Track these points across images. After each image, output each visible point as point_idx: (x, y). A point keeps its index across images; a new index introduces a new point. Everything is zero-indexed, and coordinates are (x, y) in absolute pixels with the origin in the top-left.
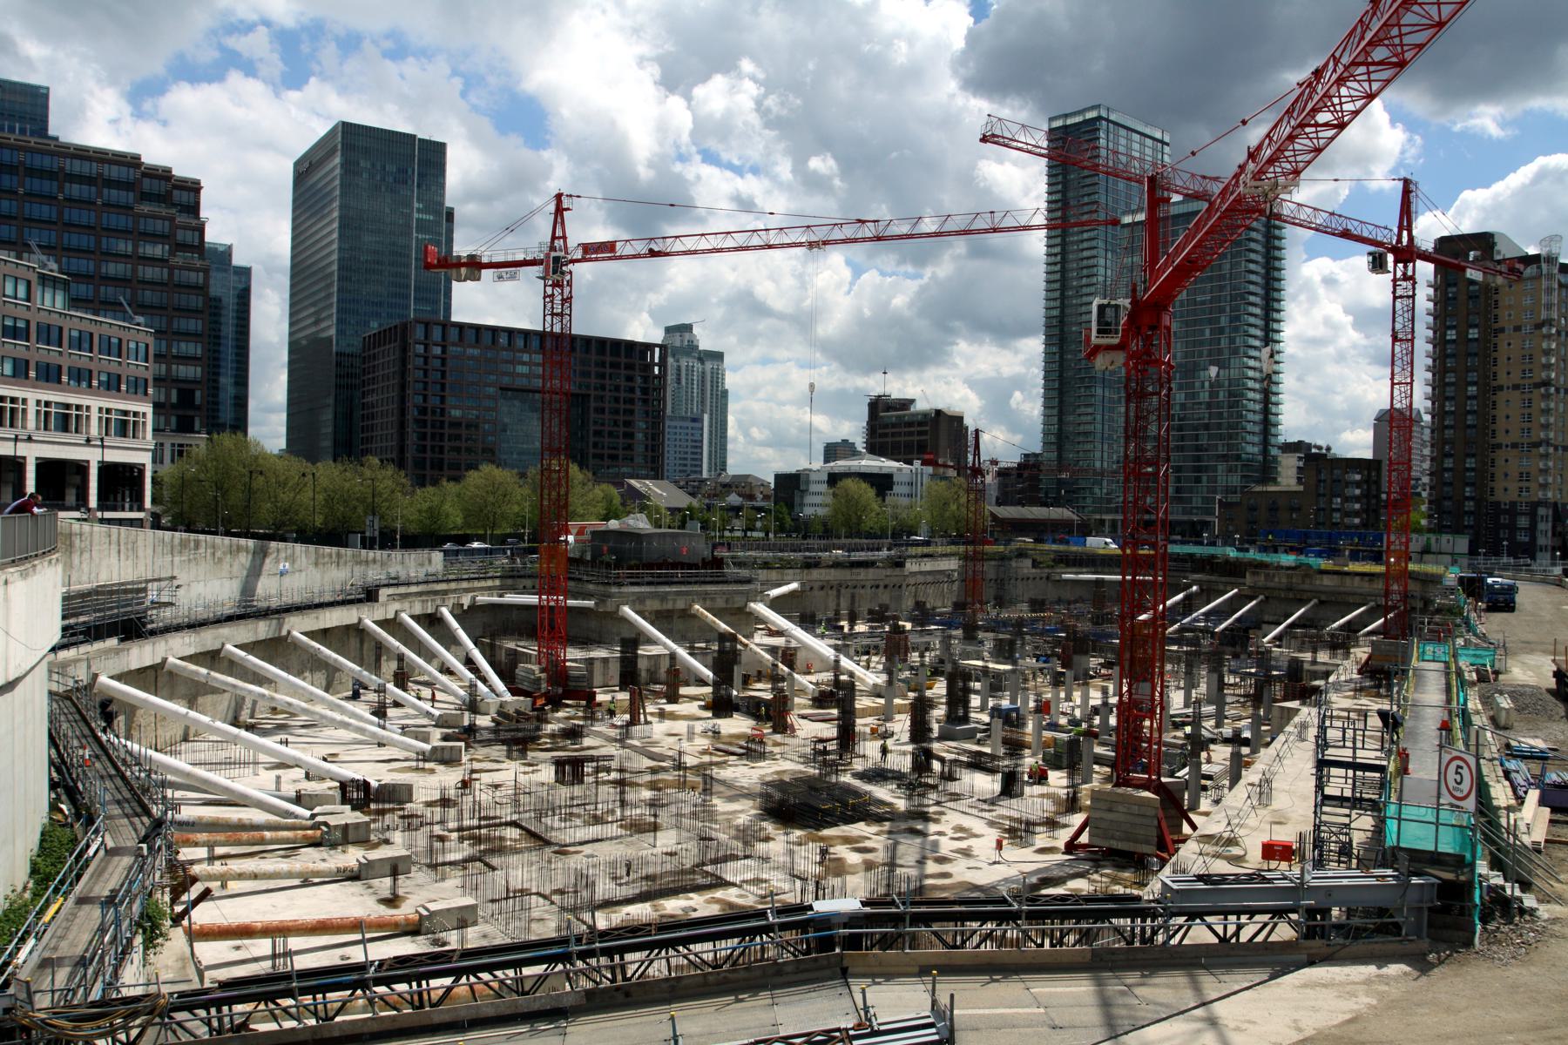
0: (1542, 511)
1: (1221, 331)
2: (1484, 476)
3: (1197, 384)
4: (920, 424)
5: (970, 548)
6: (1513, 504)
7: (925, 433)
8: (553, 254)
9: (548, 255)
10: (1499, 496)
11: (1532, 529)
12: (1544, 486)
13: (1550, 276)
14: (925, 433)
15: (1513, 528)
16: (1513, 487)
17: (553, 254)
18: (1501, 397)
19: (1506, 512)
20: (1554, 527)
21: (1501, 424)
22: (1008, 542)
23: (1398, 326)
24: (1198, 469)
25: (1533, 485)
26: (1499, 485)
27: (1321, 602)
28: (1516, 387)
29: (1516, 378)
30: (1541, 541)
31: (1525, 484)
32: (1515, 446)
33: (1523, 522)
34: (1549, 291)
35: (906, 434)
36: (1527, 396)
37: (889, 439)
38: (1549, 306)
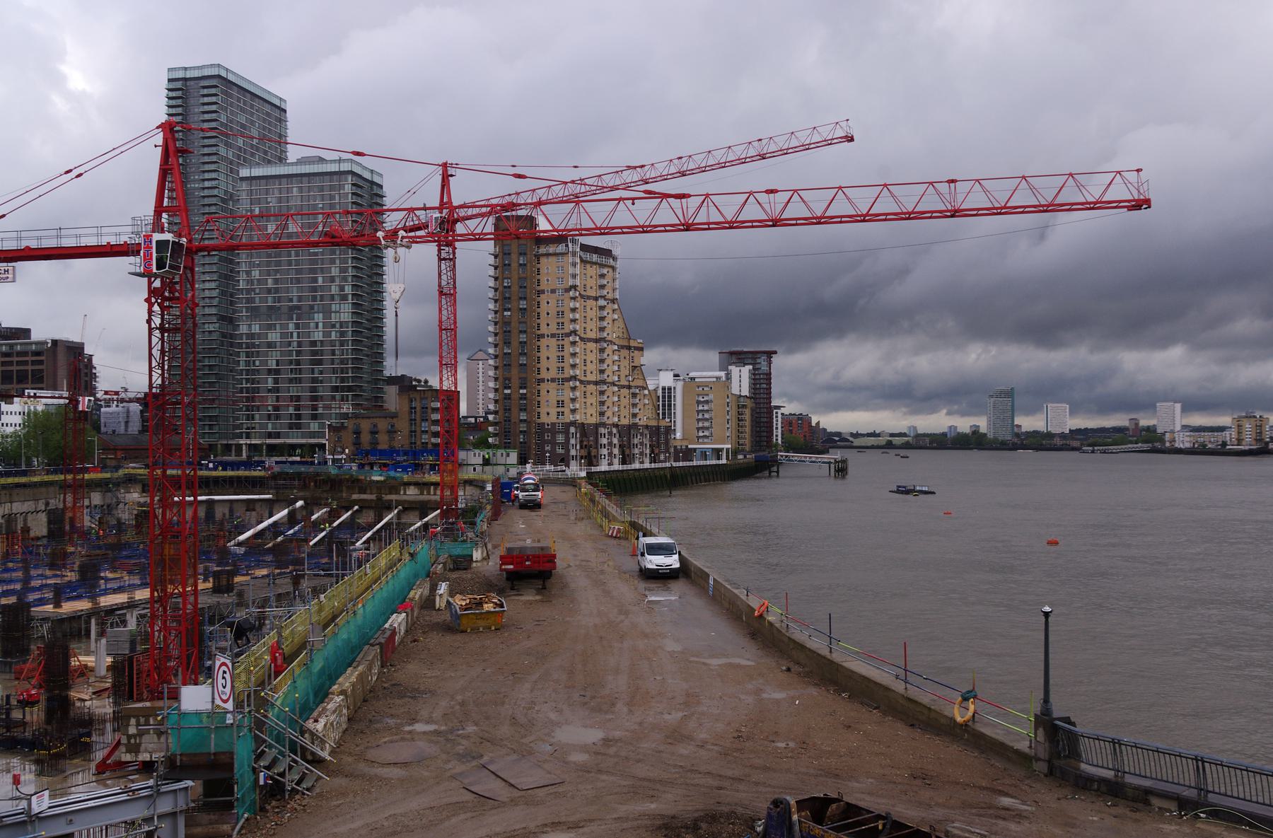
0: (572, 430)
1: (332, 279)
2: (529, 404)
3: (312, 325)
4: (38, 353)
5: (69, 477)
6: (553, 424)
7: (41, 362)
8: (157, 237)
9: (148, 238)
10: (544, 419)
11: (566, 445)
12: (574, 411)
13: (574, 254)
14: (41, 362)
15: (554, 443)
16: (553, 411)
17: (157, 237)
18: (544, 342)
19: (548, 431)
20: (581, 442)
21: (544, 364)
22: (117, 468)
23: (444, 283)
24: (314, 399)
25: (567, 411)
26: (543, 411)
27: (405, 509)
28: (553, 336)
29: (553, 328)
30: (573, 452)
31: (560, 410)
32: (553, 380)
33: (560, 438)
34: (574, 265)
35: (34, 363)
36: (561, 343)
37: (15, 368)
38: (574, 276)
